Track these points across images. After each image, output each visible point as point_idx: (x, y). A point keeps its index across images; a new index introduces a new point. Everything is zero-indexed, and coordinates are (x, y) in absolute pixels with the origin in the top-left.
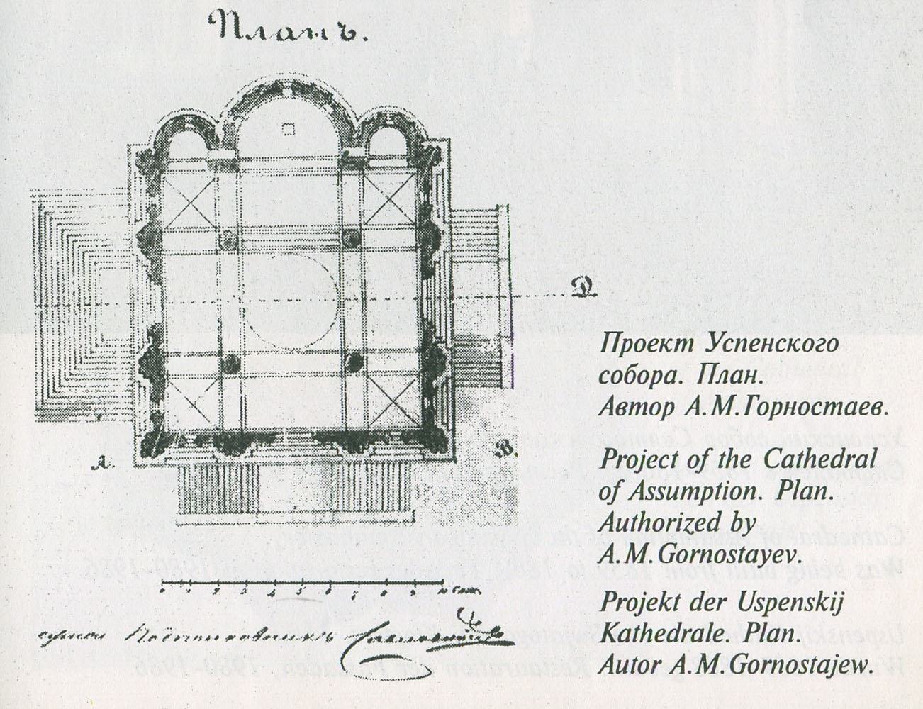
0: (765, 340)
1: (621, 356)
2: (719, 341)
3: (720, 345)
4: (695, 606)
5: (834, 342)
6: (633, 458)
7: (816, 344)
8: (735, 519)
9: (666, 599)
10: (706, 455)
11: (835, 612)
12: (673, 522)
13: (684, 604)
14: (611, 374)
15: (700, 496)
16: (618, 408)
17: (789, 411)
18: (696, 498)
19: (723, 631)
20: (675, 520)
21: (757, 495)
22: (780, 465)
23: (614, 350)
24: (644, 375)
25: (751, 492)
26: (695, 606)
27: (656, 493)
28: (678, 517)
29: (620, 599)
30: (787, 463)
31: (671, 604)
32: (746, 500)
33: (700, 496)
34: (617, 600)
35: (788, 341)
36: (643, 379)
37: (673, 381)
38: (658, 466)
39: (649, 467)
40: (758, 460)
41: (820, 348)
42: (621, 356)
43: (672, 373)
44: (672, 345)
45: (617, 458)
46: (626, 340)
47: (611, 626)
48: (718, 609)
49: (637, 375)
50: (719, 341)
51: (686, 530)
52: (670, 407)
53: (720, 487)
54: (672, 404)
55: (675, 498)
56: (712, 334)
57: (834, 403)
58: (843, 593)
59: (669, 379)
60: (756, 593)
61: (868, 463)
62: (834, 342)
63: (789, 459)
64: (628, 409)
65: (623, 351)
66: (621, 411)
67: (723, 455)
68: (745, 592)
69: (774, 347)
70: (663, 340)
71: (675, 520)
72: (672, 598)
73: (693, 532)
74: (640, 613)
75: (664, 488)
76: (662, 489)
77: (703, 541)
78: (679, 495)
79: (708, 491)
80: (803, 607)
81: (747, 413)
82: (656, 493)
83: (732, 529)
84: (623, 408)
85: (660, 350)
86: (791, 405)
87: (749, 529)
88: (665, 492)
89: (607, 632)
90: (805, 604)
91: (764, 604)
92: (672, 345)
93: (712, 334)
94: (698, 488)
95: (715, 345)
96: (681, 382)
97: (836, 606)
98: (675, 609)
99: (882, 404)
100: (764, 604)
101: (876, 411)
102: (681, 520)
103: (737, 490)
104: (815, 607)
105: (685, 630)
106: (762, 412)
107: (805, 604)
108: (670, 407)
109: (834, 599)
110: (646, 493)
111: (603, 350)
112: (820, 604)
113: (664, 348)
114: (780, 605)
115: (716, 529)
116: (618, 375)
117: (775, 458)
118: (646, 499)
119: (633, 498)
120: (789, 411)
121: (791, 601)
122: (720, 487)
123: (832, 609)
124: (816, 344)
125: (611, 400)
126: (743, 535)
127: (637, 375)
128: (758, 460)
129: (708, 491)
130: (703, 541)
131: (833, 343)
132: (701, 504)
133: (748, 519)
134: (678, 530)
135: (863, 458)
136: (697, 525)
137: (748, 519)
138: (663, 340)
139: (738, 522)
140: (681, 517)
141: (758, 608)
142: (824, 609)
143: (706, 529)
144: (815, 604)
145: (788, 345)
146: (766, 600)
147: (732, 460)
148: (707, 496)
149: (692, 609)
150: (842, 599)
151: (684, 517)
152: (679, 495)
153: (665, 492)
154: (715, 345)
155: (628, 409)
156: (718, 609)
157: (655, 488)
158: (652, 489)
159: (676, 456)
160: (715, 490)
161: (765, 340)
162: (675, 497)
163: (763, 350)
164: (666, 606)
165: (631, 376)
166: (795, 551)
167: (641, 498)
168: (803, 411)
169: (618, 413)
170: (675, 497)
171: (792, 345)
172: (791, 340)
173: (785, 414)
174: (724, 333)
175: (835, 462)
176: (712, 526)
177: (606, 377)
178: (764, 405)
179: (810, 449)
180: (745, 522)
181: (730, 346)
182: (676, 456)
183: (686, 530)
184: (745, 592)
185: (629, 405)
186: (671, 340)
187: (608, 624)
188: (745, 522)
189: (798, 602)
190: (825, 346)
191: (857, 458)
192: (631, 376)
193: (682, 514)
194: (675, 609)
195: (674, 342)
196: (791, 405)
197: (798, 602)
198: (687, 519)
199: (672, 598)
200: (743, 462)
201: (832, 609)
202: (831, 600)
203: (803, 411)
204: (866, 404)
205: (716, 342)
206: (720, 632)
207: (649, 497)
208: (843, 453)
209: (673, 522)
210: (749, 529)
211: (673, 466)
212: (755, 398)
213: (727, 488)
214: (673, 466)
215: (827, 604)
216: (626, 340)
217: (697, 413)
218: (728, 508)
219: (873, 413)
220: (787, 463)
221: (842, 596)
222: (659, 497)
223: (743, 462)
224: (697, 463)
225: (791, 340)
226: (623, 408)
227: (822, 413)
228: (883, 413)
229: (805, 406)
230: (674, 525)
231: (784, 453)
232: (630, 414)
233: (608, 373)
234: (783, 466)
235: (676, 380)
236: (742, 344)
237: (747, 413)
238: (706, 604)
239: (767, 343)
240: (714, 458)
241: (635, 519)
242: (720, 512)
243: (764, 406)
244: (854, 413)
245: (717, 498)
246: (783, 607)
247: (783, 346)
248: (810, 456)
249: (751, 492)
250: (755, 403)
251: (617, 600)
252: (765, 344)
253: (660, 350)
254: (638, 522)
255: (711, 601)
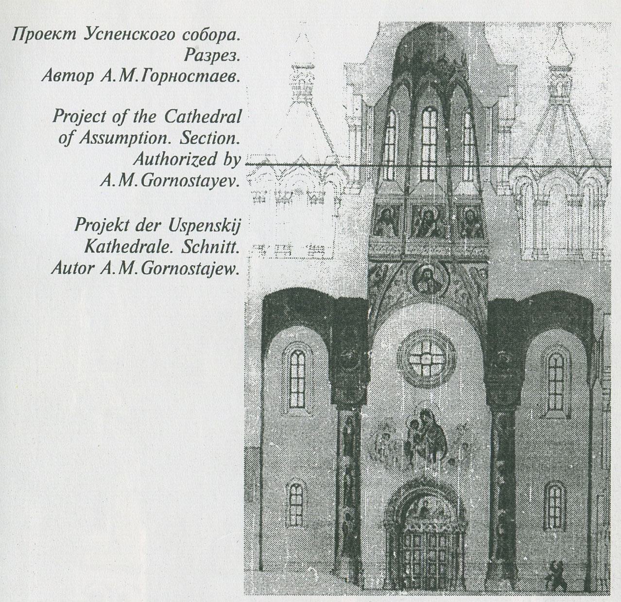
0: (125, 32)
1: (26, 42)
2: (94, 32)
3: (95, 35)
4: (139, 228)
5: (172, 34)
6: (75, 116)
7: (160, 35)
8: (227, 157)
9: (226, 224)
10: (125, 114)
11: (235, 232)
12: (184, 159)
13: (132, 227)
14: (191, 34)
15: (129, 141)
16: (55, 76)
17: (172, 79)
18: (126, 142)
19: (168, 245)
20: (186, 157)
21: (235, 141)
22: (176, 120)
23: (21, 39)
24: (213, 34)
25: (163, 138)
26: (139, 228)
27: (98, 139)
28: (188, 155)
29: (88, 223)
30: (180, 119)
31: (123, 226)
32: (228, 144)
33: (129, 141)
34: (86, 224)
35: (141, 33)
36: (212, 37)
37: (233, 39)
38: (92, 121)
39: (86, 121)
40: (161, 117)
41: (163, 38)
42: (26, 42)
43: (233, 34)
44: (61, 35)
45: (64, 115)
46: (29, 32)
47: (91, 242)
48: (155, 230)
49: (209, 35)
50: (94, 32)
51: (193, 164)
52: (90, 76)
53: (142, 135)
54: (93, 73)
55: (111, 143)
56: (89, 28)
57: (203, 74)
58: (240, 220)
59: (231, 37)
60: (181, 220)
61: (236, 120)
62: (172, 34)
63: (101, 246)
64: (61, 77)
65: (27, 39)
66: (57, 79)
67: (137, 114)
68: (174, 218)
69: (131, 36)
70: (55, 32)
71: (186, 157)
72: (123, 222)
73: (198, 166)
74: (101, 233)
75: (104, 136)
76: (102, 136)
77: (205, 171)
78: (114, 140)
79: (134, 138)
80: (213, 229)
81: (143, 80)
82: (98, 139)
83: (225, 164)
84: (59, 76)
85: (53, 39)
86: (174, 75)
87: (236, 163)
88: (104, 139)
89: (89, 245)
90: (215, 227)
91: (187, 227)
92: (61, 35)
93: (89, 28)
94: (127, 136)
95: (91, 35)
96: (238, 39)
97: (236, 228)
98: (126, 230)
99: (235, 74)
100: (187, 227)
101: (231, 79)
102: (189, 157)
103: (154, 137)
104: (221, 228)
105: (142, 245)
106: (154, 79)
107: (215, 227)
108: (90, 76)
109: (234, 224)
110: (91, 139)
111: (14, 39)
112: (224, 227)
113: (55, 37)
114: (198, 227)
115: (214, 164)
116: (195, 34)
117: (172, 116)
118: (92, 143)
119: (82, 142)
120: (172, 79)
121: (205, 225)
122: (142, 135)
123: (233, 230)
124: (160, 35)
125: (50, 71)
126: (232, 168)
127: (209, 35)
128: (161, 117)
129: (134, 138)
130: (205, 171)
131: (172, 34)
132: (129, 146)
133: (235, 157)
134: (188, 164)
135: (232, 116)
136: (200, 161)
137: (235, 157)
138: (55, 32)
139: (228, 159)
140: (189, 155)
141: (183, 229)
142: (228, 231)
143: (207, 164)
144: (221, 227)
145: (140, 36)
146: (188, 224)
147: (142, 116)
148: (133, 141)
149: (137, 230)
150: (239, 224)
151: (192, 156)
152: (114, 140)
153: (104, 139)
154: (91, 35)
155: (61, 77)
156: (155, 230)
157: (97, 136)
158: (95, 136)
159: (104, 114)
160: (139, 137)
161: (125, 32)
162: (111, 142)
163: (123, 39)
164: (227, 229)
165: (204, 36)
166: (235, 178)
167: (88, 142)
168: (182, 79)
169: (55, 80)
170: (111, 142)
171: (143, 35)
172: (143, 32)
173: (169, 81)
174: (97, 27)
175: (180, 119)
176: (211, 162)
177: (187, 36)
178: (155, 75)
179: (143, 110)
180: (233, 159)
181: (101, 36)
182: (104, 114)
183: (193, 164)
184: (174, 218)
185: (63, 74)
186: (60, 31)
187: (89, 240)
188: (233, 159)
189: (210, 226)
190: (166, 36)
191: (228, 116)
192: (204, 36)
193: (190, 153)
194: (126, 230)
195: (63, 33)
196: (174, 75)
197: (210, 226)
198: (194, 157)
199: (123, 222)
200: (151, 119)
201: (233, 230)
202: (232, 224)
203: (182, 79)
204: (225, 75)
205: (92, 33)
206: (166, 246)
207: (94, 141)
208: (219, 113)
209: (184, 159)
210: (236, 163)
211: (102, 121)
212: (149, 70)
213: (215, 136)
214: (102, 121)
215: (230, 227)
216: (29, 32)
217: (110, 80)
218: (222, 149)
219: (229, 80)
220: (180, 119)
221: (240, 222)
222: (100, 141)
223: (151, 119)
224: (120, 118)
225: (143, 32)
226: (59, 76)
227: (195, 80)
228: (236, 80)
229: (183, 76)
230: (185, 161)
231: (179, 113)
232: (63, 80)
233: (189, 33)
234: (178, 121)
235: (235, 37)
236: (109, 34)
237: (143, 80)
238: (147, 227)
239: (126, 34)
240: (130, 116)
241: (158, 156)
242: (217, 152)
243: (155, 75)
244: (216, 80)
245: (140, 142)
246: (149, 229)
247: (137, 36)
248: (143, 114)
249: (163, 138)
250: (149, 73)
251: (86, 224)
252: (125, 35)
253: (53, 39)
254: (160, 158)
255: (111, 224)
